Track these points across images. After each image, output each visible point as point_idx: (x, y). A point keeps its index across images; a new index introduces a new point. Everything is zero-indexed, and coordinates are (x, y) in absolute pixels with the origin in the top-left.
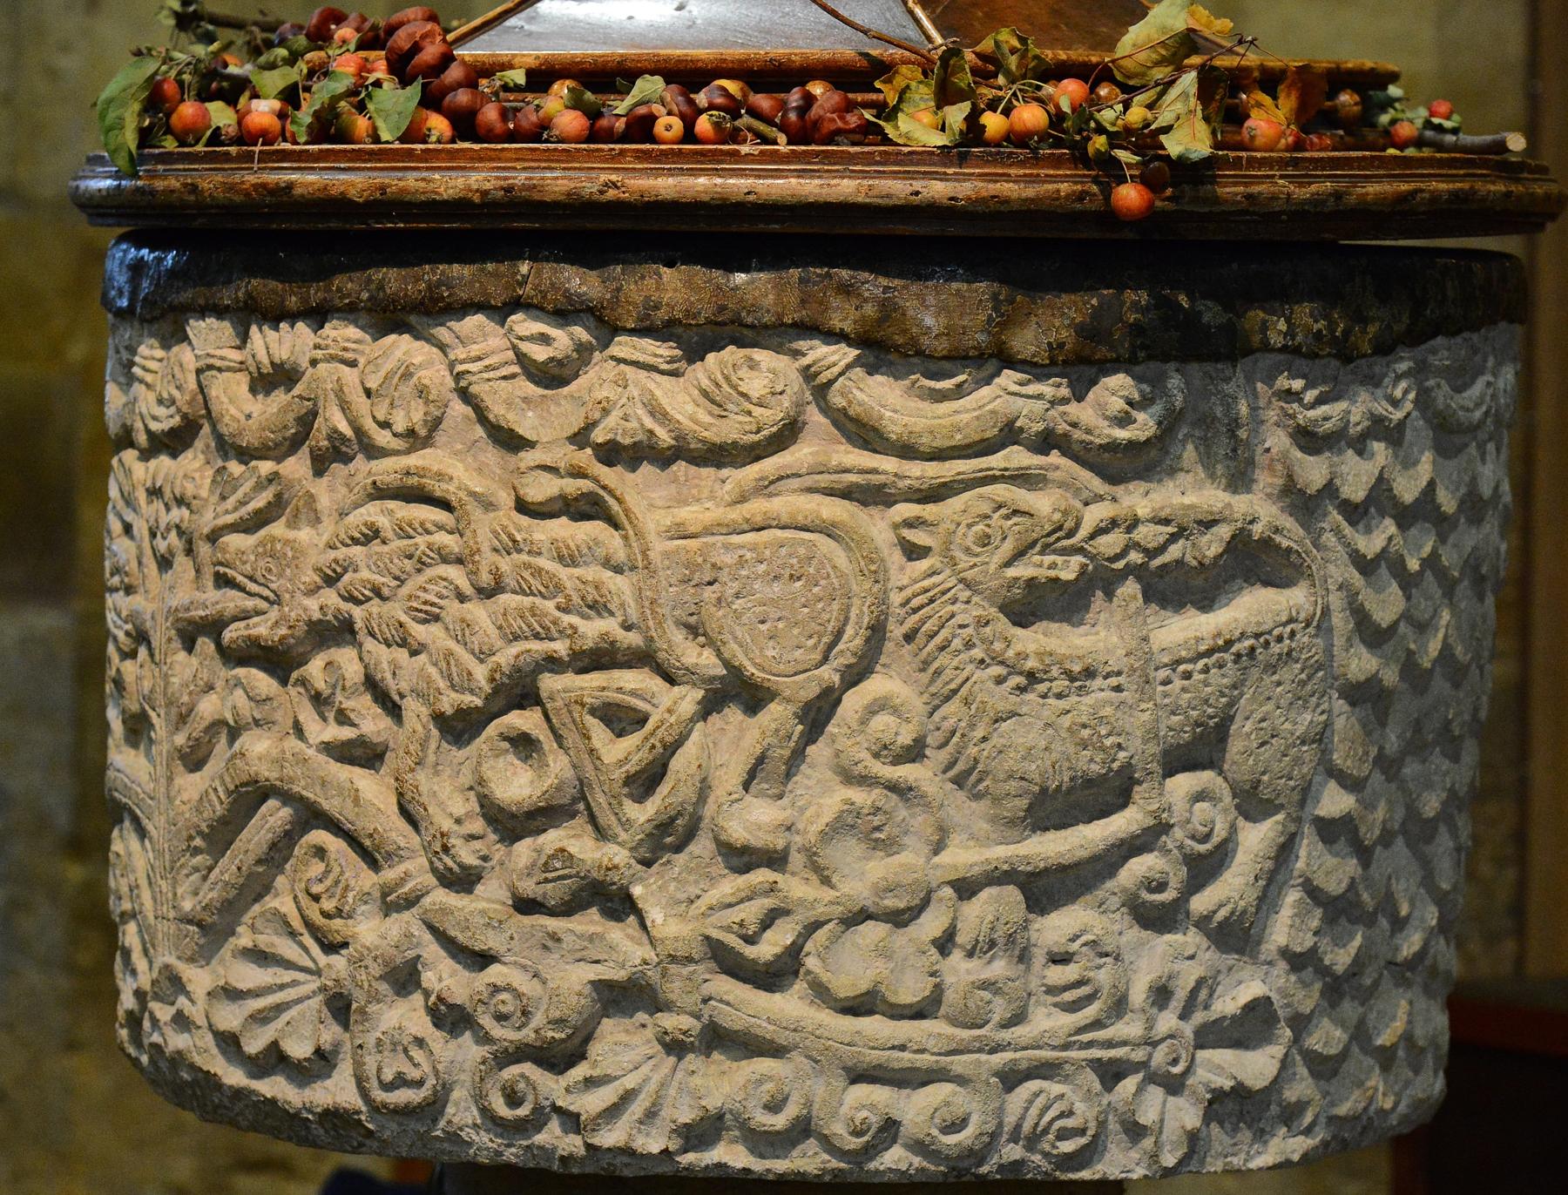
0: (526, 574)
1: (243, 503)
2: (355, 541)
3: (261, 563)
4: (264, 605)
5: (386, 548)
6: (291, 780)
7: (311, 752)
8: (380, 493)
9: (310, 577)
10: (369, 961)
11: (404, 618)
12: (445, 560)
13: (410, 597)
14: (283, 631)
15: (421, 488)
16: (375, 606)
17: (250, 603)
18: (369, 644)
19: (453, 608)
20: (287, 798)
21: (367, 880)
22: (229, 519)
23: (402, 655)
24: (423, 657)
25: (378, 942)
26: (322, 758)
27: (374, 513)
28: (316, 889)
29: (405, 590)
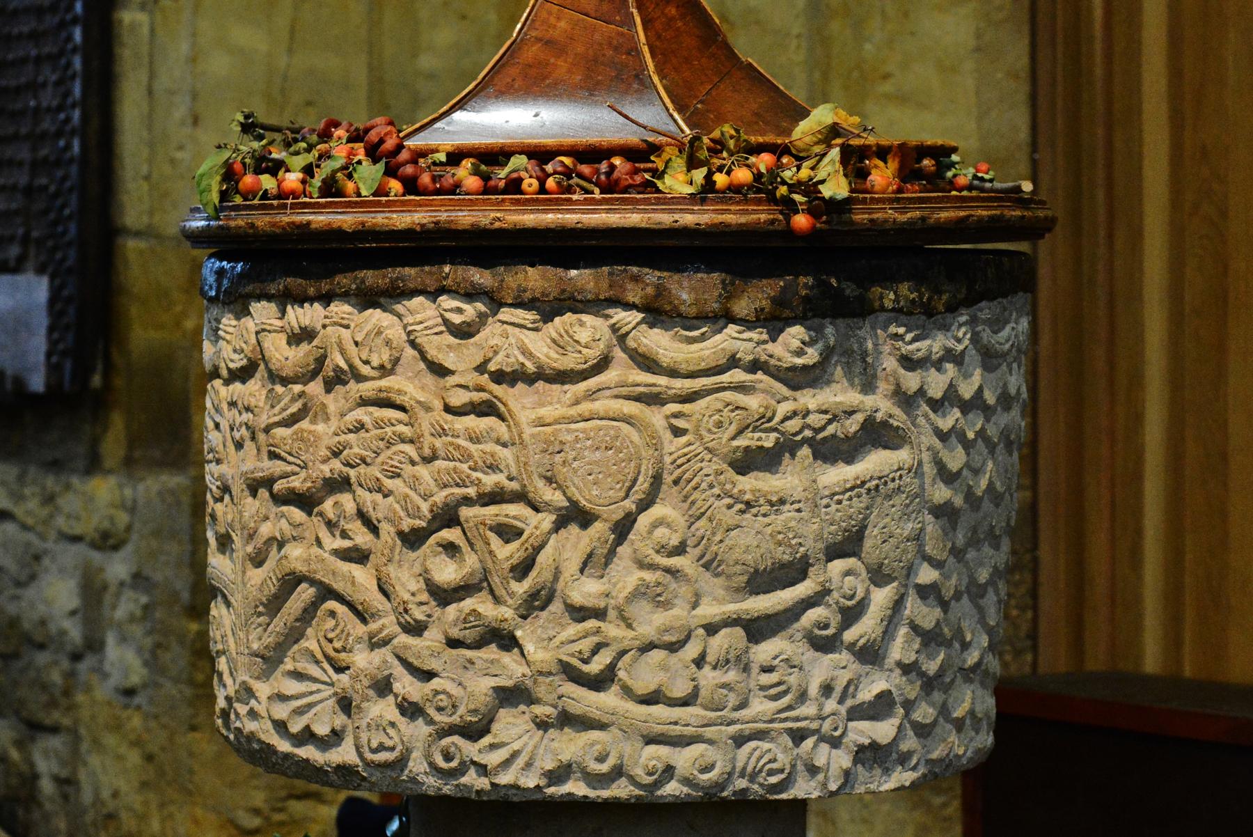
0: (451, 449)
1: (284, 410)
2: (350, 431)
3: (296, 445)
4: (297, 469)
5: (368, 435)
6: (315, 572)
7: (326, 555)
8: (364, 402)
9: (324, 452)
10: (362, 678)
11: (379, 476)
12: (403, 441)
13: (383, 463)
14: (309, 484)
15: (389, 399)
16: (362, 469)
17: (289, 468)
18: (359, 491)
19: (408, 469)
20: (312, 582)
21: (360, 629)
22: (277, 419)
23: (379, 497)
24: (391, 499)
25: (367, 666)
26: (333, 558)
27: (361, 414)
28: (330, 635)
29: (380, 459)
